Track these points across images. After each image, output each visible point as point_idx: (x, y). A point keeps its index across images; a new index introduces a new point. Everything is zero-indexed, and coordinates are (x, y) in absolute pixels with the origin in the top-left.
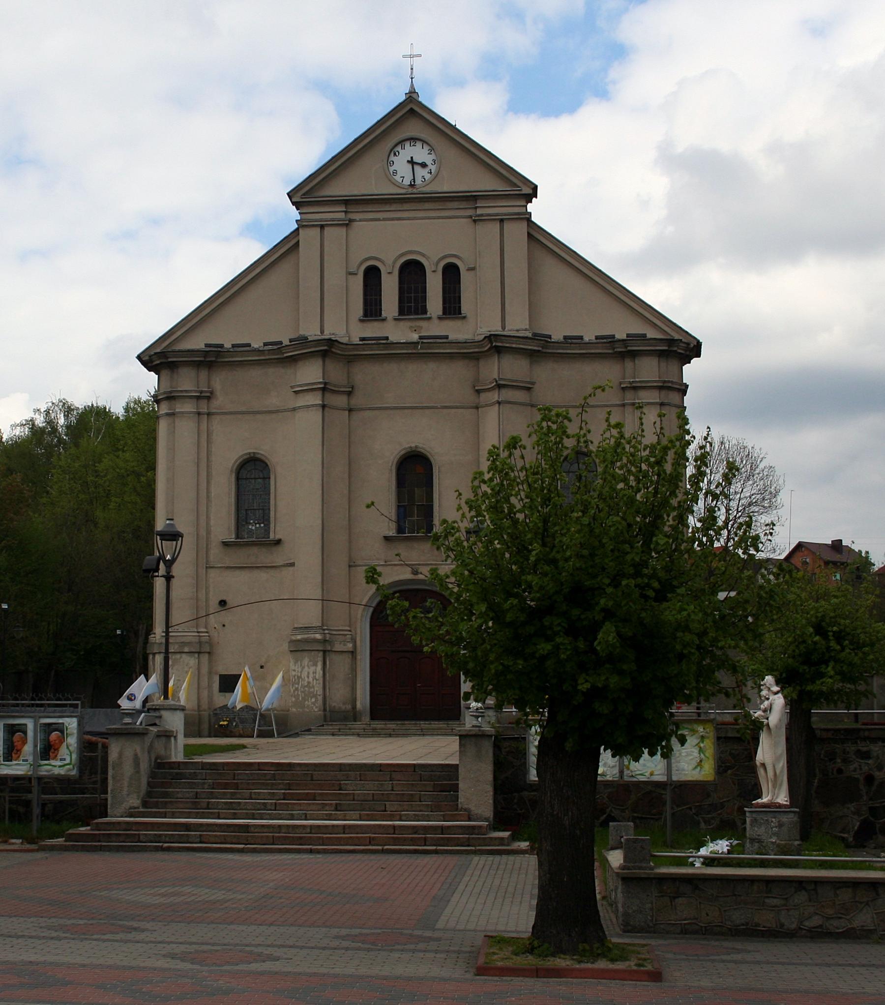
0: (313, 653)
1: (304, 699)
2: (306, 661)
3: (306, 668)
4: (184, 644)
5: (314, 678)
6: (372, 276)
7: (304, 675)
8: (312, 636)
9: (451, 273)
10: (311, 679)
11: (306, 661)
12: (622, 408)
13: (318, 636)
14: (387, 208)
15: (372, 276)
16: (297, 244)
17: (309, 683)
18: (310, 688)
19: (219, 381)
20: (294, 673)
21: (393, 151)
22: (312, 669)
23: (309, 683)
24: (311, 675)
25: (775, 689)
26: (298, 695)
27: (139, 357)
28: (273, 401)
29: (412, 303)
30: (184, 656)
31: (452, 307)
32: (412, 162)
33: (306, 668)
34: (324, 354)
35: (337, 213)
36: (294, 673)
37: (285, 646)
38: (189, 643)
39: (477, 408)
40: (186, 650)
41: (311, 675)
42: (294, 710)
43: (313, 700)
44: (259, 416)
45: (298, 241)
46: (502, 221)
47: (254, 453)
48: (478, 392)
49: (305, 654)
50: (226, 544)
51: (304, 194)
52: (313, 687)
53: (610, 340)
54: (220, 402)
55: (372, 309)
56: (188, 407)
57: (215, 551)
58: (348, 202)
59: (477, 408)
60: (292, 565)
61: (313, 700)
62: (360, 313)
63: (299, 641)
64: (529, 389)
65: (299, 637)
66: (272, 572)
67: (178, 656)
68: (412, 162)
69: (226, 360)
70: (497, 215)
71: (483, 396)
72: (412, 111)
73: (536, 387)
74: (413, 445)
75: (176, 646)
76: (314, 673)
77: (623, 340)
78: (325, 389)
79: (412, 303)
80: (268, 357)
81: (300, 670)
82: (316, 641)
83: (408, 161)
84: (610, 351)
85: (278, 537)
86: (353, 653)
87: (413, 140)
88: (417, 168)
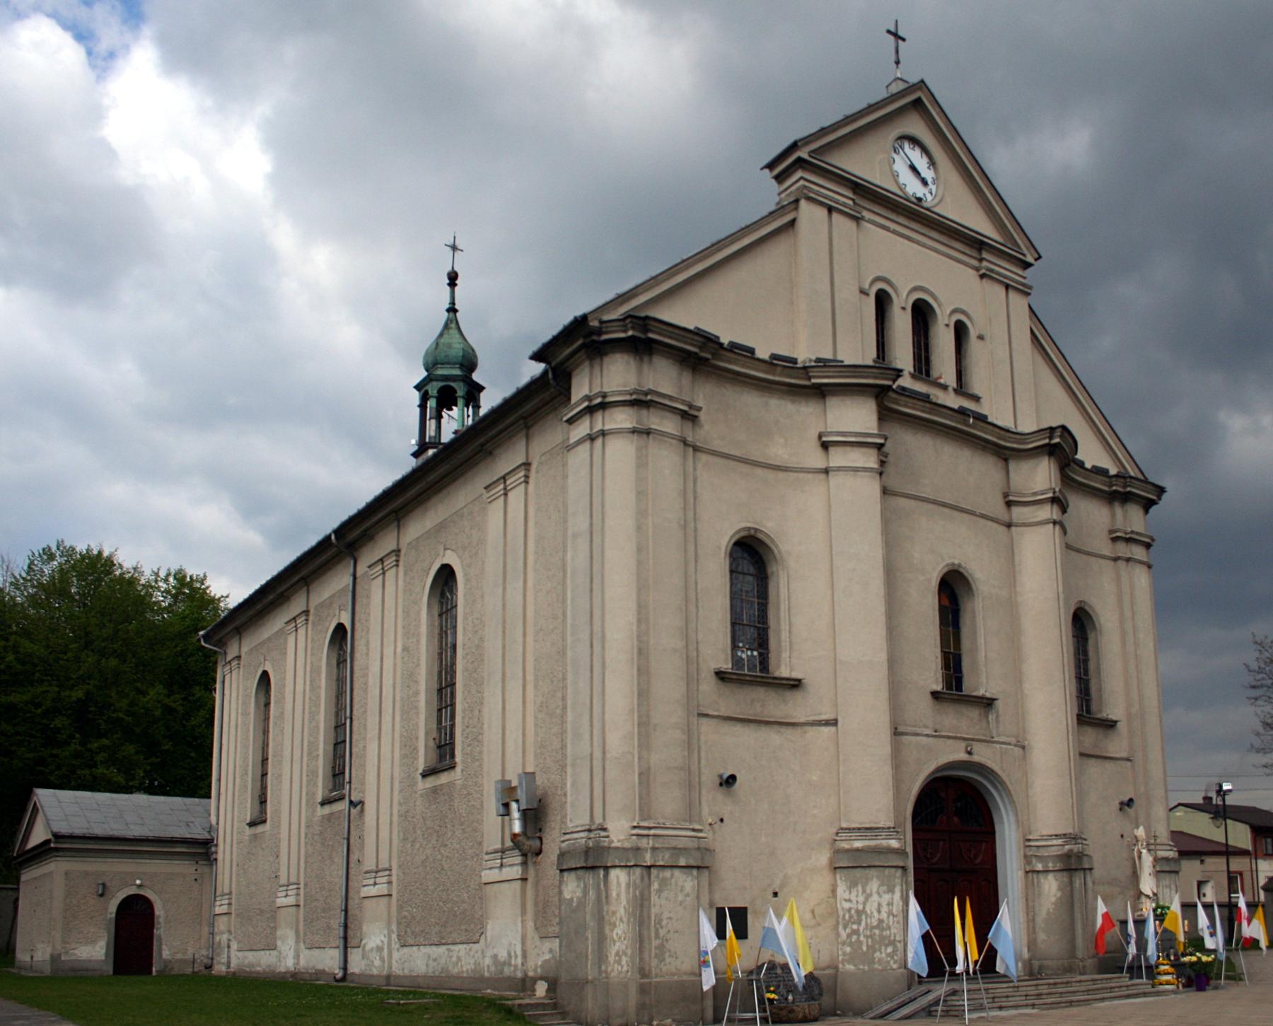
0: (887, 871)
1: (872, 949)
2: (874, 885)
3: (875, 897)
4: (678, 851)
5: (890, 913)
6: (882, 301)
7: (871, 907)
8: (884, 843)
10: (884, 915)
11: (874, 885)
12: (822, 476)
13: (894, 844)
14: (901, 220)
17: (881, 921)
18: (883, 929)
19: (704, 395)
20: (847, 905)
22: (887, 897)
23: (881, 921)
24: (885, 909)
26: (859, 942)
28: (778, 452)
30: (677, 872)
33: (875, 897)
35: (843, 197)
36: (847, 905)
37: (823, 858)
38: (684, 850)
39: (1009, 525)
40: (682, 862)
41: (885, 909)
42: (850, 967)
43: (890, 950)
44: (759, 471)
47: (756, 530)
48: (1009, 504)
49: (873, 872)
50: (721, 675)
51: (813, 151)
52: (889, 928)
53: (788, 363)
54: (710, 431)
56: (669, 424)
57: (708, 685)
58: (861, 190)
59: (1009, 525)
60: (1082, 755)
61: (890, 950)
63: (857, 850)
65: (858, 844)
66: (788, 732)
67: (668, 873)
69: (727, 365)
70: (1006, 277)
71: (1016, 511)
72: (917, 103)
73: (1154, 544)
74: (956, 562)
75: (667, 856)
76: (890, 904)
77: (721, 345)
80: (777, 378)
81: (861, 899)
82: (891, 851)
84: (1106, 488)
85: (795, 675)
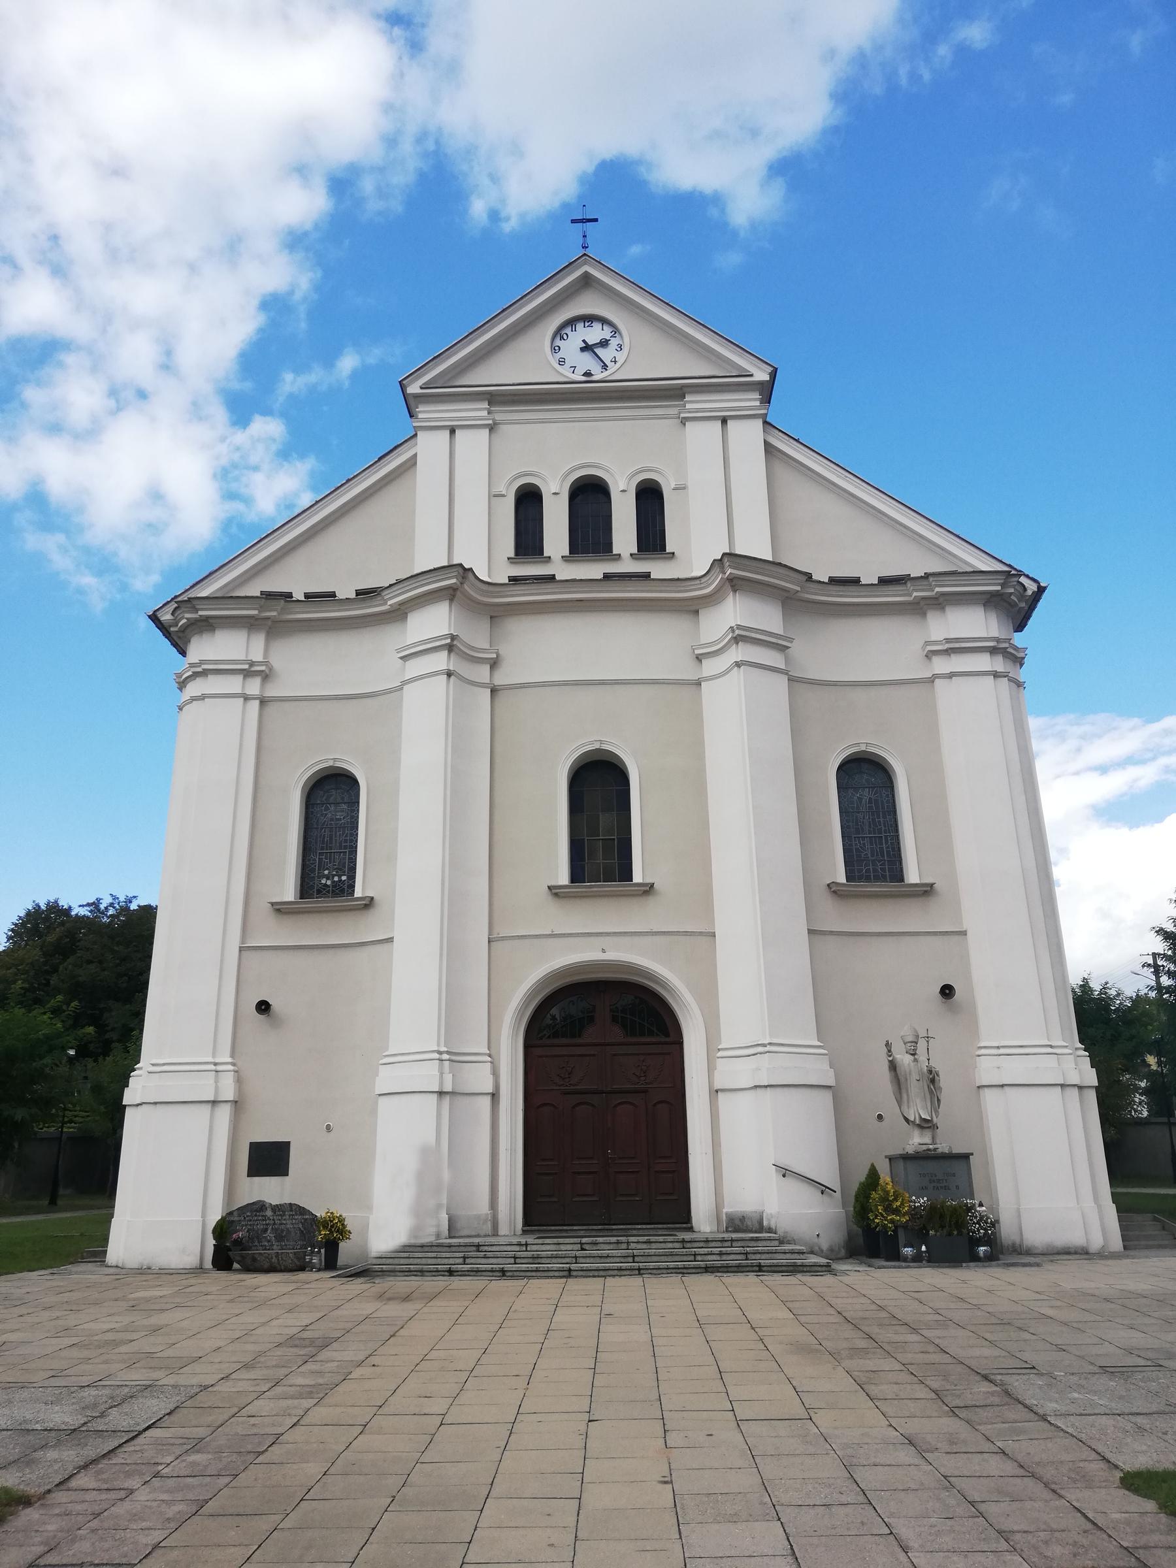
6: (529, 501)
9: (650, 497)
15: (529, 501)
16: (412, 462)
21: (559, 333)
25: (21, 1487)
27: (288, 1143)
29: (590, 536)
31: (652, 538)
32: (587, 348)
34: (450, 594)
35: (478, 411)
45: (416, 455)
46: (724, 421)
48: (699, 659)
55: (528, 542)
58: (497, 398)
62: (511, 553)
64: (783, 649)
68: (587, 348)
78: (451, 646)
79: (590, 536)
83: (582, 350)
86: (495, 1096)
87: (589, 319)
88: (599, 351)
